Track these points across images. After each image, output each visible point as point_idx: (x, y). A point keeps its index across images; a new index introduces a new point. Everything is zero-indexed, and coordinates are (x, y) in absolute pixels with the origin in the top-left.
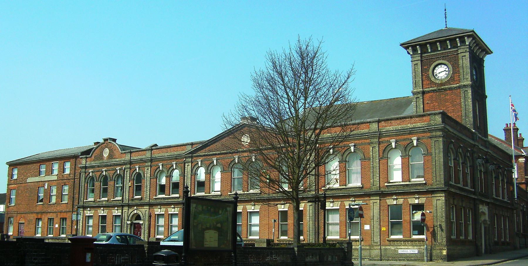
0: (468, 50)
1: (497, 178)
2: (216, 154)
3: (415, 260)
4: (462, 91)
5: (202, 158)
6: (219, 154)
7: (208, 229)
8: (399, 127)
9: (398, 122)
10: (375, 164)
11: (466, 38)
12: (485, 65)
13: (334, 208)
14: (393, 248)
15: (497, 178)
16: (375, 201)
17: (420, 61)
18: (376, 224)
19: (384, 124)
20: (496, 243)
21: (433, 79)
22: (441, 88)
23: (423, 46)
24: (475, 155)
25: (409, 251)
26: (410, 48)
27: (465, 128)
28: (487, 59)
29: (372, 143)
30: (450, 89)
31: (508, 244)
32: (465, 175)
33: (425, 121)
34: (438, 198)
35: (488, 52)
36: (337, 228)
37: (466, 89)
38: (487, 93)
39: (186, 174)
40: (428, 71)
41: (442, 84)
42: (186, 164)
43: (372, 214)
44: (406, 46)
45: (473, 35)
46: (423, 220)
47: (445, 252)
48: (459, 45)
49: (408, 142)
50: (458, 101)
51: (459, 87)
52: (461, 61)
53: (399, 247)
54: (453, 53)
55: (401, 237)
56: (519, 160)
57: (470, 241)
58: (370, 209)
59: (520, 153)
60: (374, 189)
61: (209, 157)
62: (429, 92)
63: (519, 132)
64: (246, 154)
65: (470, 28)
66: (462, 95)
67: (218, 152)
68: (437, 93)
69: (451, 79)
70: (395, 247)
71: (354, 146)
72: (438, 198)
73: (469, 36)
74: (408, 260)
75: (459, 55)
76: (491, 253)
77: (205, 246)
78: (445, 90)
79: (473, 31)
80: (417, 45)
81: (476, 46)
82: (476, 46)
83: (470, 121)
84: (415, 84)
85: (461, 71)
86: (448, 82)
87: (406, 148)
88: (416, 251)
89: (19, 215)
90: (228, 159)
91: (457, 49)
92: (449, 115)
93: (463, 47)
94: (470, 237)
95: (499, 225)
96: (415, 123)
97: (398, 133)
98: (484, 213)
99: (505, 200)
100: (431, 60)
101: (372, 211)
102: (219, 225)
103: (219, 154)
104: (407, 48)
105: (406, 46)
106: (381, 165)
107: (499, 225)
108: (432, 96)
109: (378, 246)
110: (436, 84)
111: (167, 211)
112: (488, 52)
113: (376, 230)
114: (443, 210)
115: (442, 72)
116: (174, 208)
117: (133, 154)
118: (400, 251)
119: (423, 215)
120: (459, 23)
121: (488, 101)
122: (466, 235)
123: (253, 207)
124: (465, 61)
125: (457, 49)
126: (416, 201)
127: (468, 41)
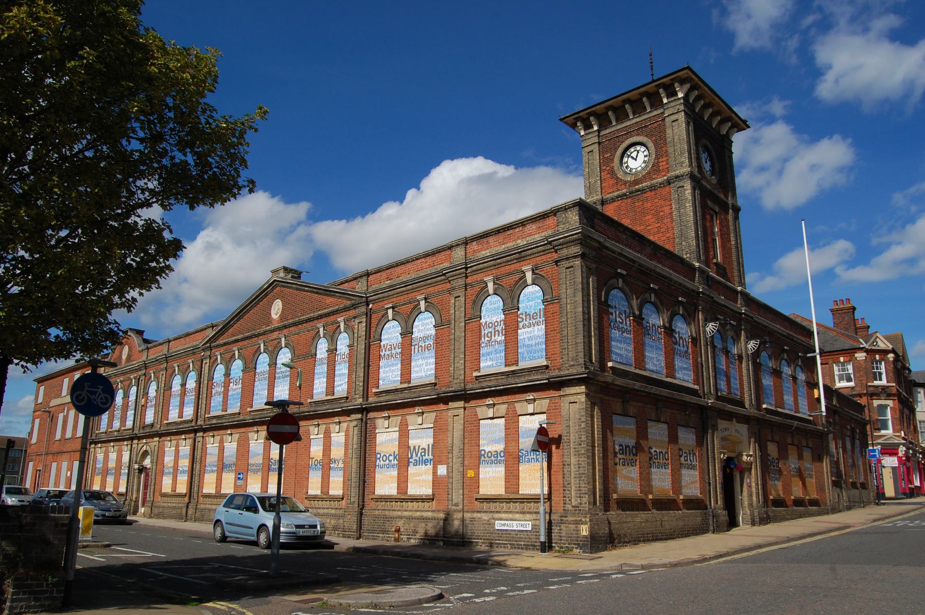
0: (682, 107)
2: (237, 341)
4: (673, 188)
5: (222, 349)
6: (242, 340)
8: (502, 248)
10: (457, 333)
16: (456, 412)
17: (597, 145)
18: (457, 466)
19: (476, 248)
21: (620, 175)
25: (515, 526)
27: (682, 260)
29: (454, 289)
30: (652, 188)
33: (549, 228)
34: (572, 399)
36: (166, 471)
37: (681, 184)
40: (612, 160)
41: (636, 182)
43: (450, 442)
47: (585, 530)
48: (665, 101)
49: (517, 277)
50: (667, 209)
51: (669, 182)
52: (669, 132)
53: (496, 515)
56: (856, 355)
58: (447, 430)
59: (856, 345)
60: (456, 386)
63: (857, 315)
66: (674, 196)
67: (240, 337)
68: (629, 200)
69: (654, 169)
70: (490, 515)
71: (425, 299)
72: (572, 399)
73: (682, 82)
75: (667, 119)
78: (642, 191)
79: (688, 68)
83: (690, 246)
85: (671, 150)
86: (648, 176)
87: (512, 291)
89: (50, 457)
91: (661, 110)
92: (651, 238)
93: (672, 104)
96: (530, 235)
97: (498, 260)
100: (616, 139)
101: (450, 434)
103: (242, 340)
106: (469, 334)
108: (619, 207)
109: (459, 511)
110: (625, 183)
111: (494, 458)
113: (457, 476)
114: (583, 425)
115: (637, 161)
116: (185, 439)
117: (151, 351)
118: (498, 525)
124: (678, 129)
125: (661, 110)
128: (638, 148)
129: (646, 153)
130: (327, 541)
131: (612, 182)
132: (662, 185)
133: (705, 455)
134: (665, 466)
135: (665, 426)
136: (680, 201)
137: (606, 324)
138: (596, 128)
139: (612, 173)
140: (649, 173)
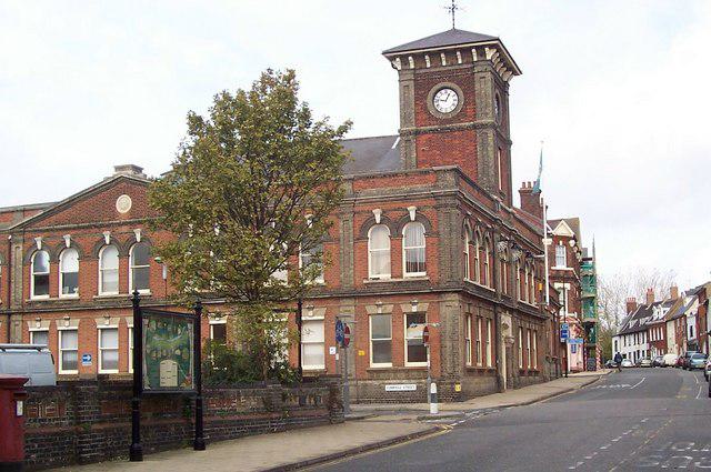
1: (522, 271)
3: (412, 402)
6: (74, 229)
7: (164, 358)
9: (386, 181)
11: (487, 49)
12: (510, 91)
13: (70, 328)
14: (376, 383)
15: (522, 271)
20: (522, 372)
22: (446, 125)
23: (419, 57)
24: (497, 236)
25: (402, 388)
26: (398, 59)
28: (515, 84)
31: (537, 372)
32: (483, 265)
35: (515, 71)
36: (320, 350)
38: (513, 137)
39: (13, 264)
42: (14, 247)
44: (391, 55)
45: (497, 45)
46: (426, 338)
49: (401, 213)
51: (475, 127)
52: (477, 86)
54: (460, 77)
55: (389, 365)
57: (490, 371)
61: (56, 234)
62: (425, 132)
64: (125, 229)
65: (495, 35)
66: (479, 140)
67: (72, 225)
69: (460, 114)
73: (491, 47)
74: (401, 402)
76: (515, 388)
77: (162, 385)
78: (452, 130)
79: (498, 39)
80: (473, 47)
81: (501, 61)
82: (501, 61)
83: (489, 182)
84: (404, 119)
85: (478, 101)
88: (414, 387)
90: (89, 239)
94: (489, 364)
95: (524, 343)
98: (506, 327)
99: (533, 305)
102: (178, 352)
104: (392, 59)
105: (391, 55)
107: (524, 343)
110: (437, 119)
111: (53, 325)
112: (515, 71)
115: (447, 102)
118: (388, 388)
119: (426, 330)
120: (476, 22)
121: (514, 150)
122: (484, 361)
123: (38, 324)
124: (484, 87)
126: (414, 309)
127: (490, 54)
128: (449, 91)
129: (456, 97)
130: (310, 372)
131: (425, 116)
132: (468, 128)
133: (510, 369)
134: (641, 320)
135: (77, 270)
136: (485, 145)
137: (474, 310)
138: (412, 66)
139: (425, 109)
140: (458, 115)
